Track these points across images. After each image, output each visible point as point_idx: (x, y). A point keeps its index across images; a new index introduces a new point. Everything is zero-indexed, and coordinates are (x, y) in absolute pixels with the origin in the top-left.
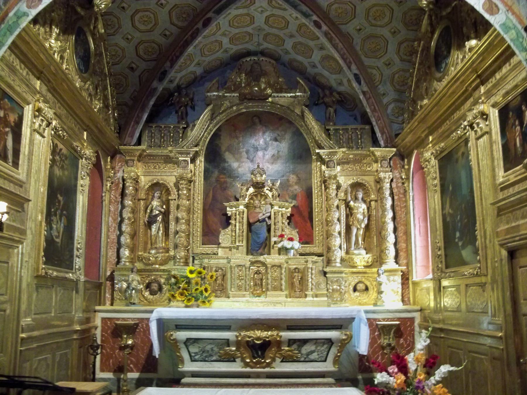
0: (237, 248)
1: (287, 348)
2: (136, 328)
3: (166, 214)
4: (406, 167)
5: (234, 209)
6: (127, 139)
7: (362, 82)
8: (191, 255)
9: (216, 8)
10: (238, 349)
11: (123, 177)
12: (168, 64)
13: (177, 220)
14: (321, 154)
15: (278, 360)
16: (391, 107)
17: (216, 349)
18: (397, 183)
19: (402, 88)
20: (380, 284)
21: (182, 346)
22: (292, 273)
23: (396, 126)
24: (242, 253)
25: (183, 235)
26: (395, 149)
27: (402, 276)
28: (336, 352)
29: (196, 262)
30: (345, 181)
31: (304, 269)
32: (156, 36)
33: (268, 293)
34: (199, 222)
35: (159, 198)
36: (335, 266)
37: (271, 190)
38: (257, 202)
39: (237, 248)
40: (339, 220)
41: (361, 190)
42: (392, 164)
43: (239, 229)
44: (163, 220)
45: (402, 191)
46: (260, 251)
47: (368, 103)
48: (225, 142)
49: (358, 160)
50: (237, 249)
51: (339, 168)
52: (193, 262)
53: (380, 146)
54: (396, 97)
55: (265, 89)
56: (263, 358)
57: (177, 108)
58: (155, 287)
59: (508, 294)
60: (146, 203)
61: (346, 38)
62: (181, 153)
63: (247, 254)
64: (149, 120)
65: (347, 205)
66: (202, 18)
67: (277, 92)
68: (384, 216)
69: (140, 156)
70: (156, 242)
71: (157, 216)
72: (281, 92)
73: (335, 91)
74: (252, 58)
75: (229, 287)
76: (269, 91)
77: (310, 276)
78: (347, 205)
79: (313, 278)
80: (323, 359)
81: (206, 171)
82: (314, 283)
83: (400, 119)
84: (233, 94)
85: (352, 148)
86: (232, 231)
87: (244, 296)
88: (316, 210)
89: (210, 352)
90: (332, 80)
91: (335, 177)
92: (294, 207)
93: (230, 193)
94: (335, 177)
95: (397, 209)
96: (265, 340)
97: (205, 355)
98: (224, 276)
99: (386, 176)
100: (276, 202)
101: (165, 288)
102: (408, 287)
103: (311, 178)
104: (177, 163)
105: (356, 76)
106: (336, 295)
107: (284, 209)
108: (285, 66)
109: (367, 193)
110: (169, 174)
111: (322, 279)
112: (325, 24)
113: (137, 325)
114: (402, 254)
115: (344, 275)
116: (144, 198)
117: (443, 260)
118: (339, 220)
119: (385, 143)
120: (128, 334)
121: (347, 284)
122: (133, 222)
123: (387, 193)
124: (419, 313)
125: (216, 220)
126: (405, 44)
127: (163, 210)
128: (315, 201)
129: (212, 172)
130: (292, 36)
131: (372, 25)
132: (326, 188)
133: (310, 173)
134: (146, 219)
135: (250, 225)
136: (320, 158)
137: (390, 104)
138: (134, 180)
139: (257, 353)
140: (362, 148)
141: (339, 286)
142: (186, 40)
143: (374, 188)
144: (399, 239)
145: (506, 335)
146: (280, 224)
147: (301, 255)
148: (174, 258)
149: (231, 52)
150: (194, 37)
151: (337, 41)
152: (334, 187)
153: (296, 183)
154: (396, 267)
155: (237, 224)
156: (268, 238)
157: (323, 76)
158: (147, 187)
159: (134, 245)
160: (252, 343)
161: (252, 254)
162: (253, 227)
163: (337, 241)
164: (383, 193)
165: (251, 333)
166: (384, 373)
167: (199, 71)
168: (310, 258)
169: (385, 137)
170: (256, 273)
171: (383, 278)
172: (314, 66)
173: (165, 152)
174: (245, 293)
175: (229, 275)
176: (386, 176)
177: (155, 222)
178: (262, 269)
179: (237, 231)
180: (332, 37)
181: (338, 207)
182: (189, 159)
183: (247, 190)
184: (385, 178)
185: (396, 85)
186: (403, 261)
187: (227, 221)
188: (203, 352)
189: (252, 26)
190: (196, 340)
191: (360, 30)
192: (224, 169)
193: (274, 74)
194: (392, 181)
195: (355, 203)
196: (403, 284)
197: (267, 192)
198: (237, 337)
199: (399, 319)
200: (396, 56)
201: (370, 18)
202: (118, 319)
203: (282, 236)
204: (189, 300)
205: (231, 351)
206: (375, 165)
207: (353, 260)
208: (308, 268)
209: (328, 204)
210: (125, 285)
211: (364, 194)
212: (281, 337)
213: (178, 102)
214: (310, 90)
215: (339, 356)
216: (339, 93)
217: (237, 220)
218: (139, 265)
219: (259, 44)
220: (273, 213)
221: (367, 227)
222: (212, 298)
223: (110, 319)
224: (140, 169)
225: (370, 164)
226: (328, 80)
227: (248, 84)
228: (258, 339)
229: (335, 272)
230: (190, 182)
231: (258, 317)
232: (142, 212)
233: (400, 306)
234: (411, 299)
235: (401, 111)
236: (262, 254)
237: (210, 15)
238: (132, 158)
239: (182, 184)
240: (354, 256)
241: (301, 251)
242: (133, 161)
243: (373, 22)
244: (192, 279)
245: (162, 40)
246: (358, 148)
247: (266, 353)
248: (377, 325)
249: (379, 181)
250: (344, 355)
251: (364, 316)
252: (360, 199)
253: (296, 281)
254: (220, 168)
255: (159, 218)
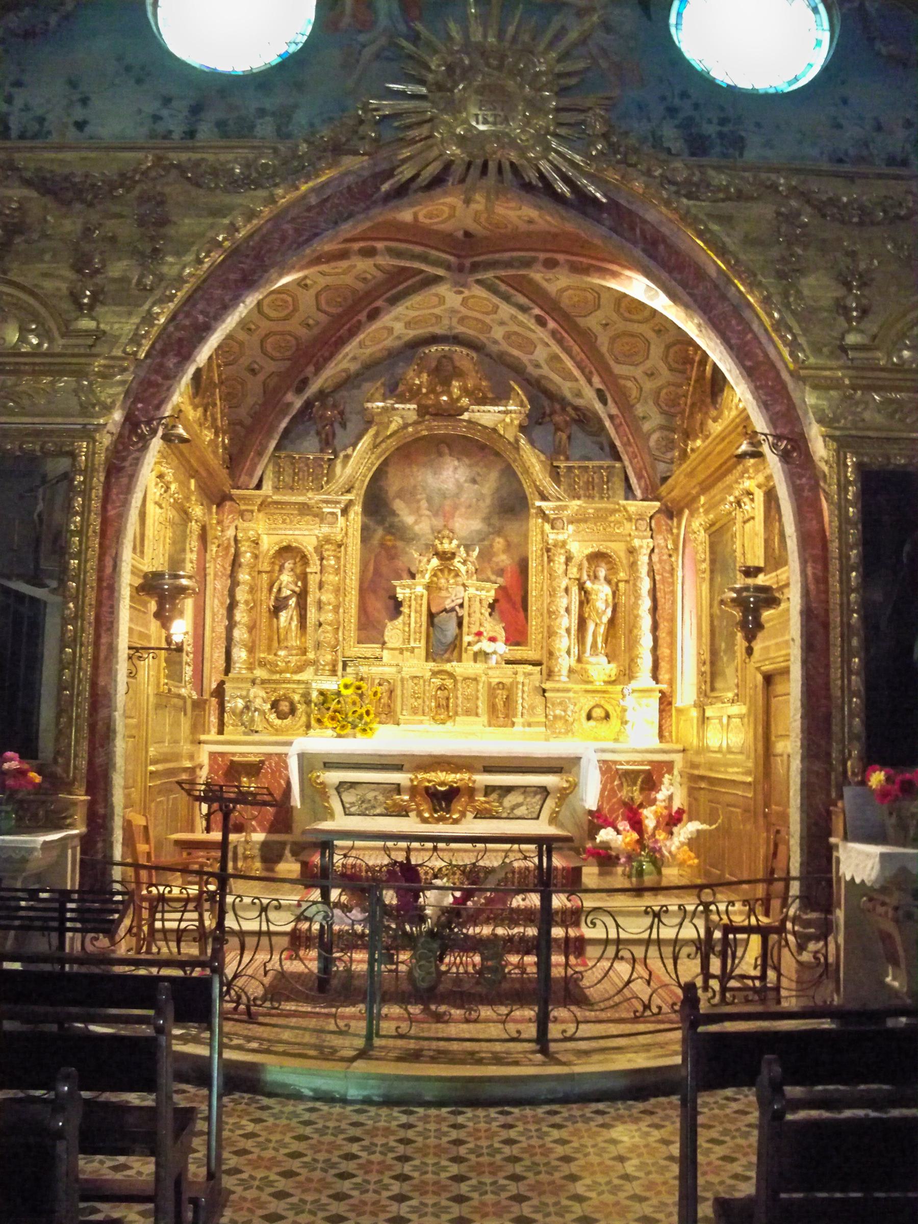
0: (412, 650)
1: (483, 799)
2: (261, 768)
3: (302, 596)
4: (675, 531)
5: (408, 591)
6: (243, 478)
7: (610, 401)
8: (340, 659)
9: (388, 295)
10: (413, 798)
11: (236, 537)
12: (311, 368)
13: (320, 605)
14: (544, 508)
15: (470, 816)
16: (655, 437)
17: (381, 798)
18: (661, 554)
19: (672, 410)
20: (624, 710)
21: (333, 793)
22: (492, 691)
23: (662, 467)
24: (419, 659)
25: (329, 628)
26: (658, 504)
27: (660, 699)
28: (554, 806)
29: (349, 670)
30: (579, 549)
31: (512, 683)
32: (294, 326)
33: (457, 718)
34: (353, 610)
35: (292, 570)
36: (558, 681)
37: (464, 563)
38: (443, 581)
39: (412, 650)
40: (567, 610)
41: (603, 565)
42: (653, 525)
43: (416, 622)
44: (298, 604)
45: (667, 568)
46: (446, 656)
47: (617, 432)
48: (393, 484)
49: (601, 517)
50: (412, 652)
51: (571, 528)
52: (344, 669)
53: (634, 498)
54: (663, 422)
55: (458, 399)
56: (448, 811)
57: (320, 427)
58: (284, 706)
59: (760, 730)
60: (270, 578)
61: (586, 338)
62: (327, 502)
63: (427, 661)
64: (278, 448)
65: (582, 587)
66: (366, 306)
67: (479, 404)
68: (636, 606)
69: (261, 505)
70: (286, 639)
71: (287, 598)
72: (485, 404)
73: (570, 404)
74: (440, 348)
75: (399, 709)
76: (465, 401)
77: (520, 694)
78: (582, 587)
79: (524, 699)
80: (535, 816)
81: (365, 528)
82: (525, 705)
83: (669, 456)
84: (408, 406)
85: (593, 497)
86: (404, 624)
87: (421, 722)
88: (533, 593)
89: (373, 802)
90: (566, 389)
91: (564, 543)
92: (502, 589)
93: (400, 564)
94: (564, 543)
95: (659, 595)
96: (451, 787)
97: (364, 806)
98: (391, 692)
99: (643, 544)
100: (472, 581)
101: (301, 708)
102: (671, 716)
103: (527, 543)
104: (320, 517)
105: (599, 393)
106: (559, 724)
107: (484, 593)
108: (491, 358)
109: (612, 568)
110: (306, 533)
111: (539, 699)
112: (553, 319)
113: (262, 762)
114: (664, 665)
115: (571, 694)
116: (268, 569)
117: (708, 680)
118: (567, 610)
119: (643, 493)
120: (248, 775)
121: (577, 709)
122: (252, 608)
123: (643, 570)
124: (681, 755)
125: (379, 605)
126: (675, 348)
127: (297, 589)
128: (532, 579)
129: (375, 531)
130: (502, 323)
131: (626, 320)
132: (550, 560)
133: (526, 537)
134: (272, 603)
135: (431, 616)
136: (542, 513)
137: (654, 431)
138: (253, 541)
139: (440, 805)
140: (608, 498)
141: (565, 711)
142: (340, 337)
143: (624, 561)
144: (660, 642)
145: (755, 781)
146: (478, 615)
147: (508, 662)
148: (314, 663)
149: (406, 338)
150: (352, 333)
151: (572, 343)
152: (562, 559)
153: (504, 552)
154: (652, 684)
155: (413, 614)
156: (459, 637)
157: (551, 380)
158: (272, 552)
159: (254, 642)
160: (432, 790)
161: (434, 661)
162: (436, 620)
163: (563, 643)
164: (637, 570)
165: (431, 776)
166: (610, 830)
167: (354, 367)
168: (520, 668)
169: (643, 484)
170: (440, 688)
171: (630, 702)
172: (538, 366)
173: (301, 499)
174: (423, 718)
175: (398, 692)
176: (643, 544)
177: (286, 607)
178: (449, 683)
179: (413, 625)
180: (563, 337)
181: (567, 590)
182: (338, 511)
183: (429, 561)
184: (641, 547)
185: (663, 405)
186: (664, 675)
187: (396, 608)
188: (363, 802)
189: (442, 307)
190: (353, 785)
191: (607, 325)
192: (392, 526)
193: (474, 374)
194: (653, 550)
195: (593, 583)
196: (661, 711)
197: (459, 565)
198: (412, 780)
199: (651, 763)
200: (662, 364)
201: (622, 310)
202: (234, 754)
203: (479, 634)
204: (343, 727)
205: (403, 800)
206: (628, 525)
207: (586, 671)
208: (518, 683)
209: (551, 585)
210: (240, 704)
211: (609, 570)
212: (474, 782)
213: (321, 417)
214: (531, 401)
215: (557, 813)
216: (576, 409)
217: (413, 608)
218: (260, 673)
219: (451, 328)
220: (466, 599)
221: (612, 622)
222: (374, 726)
223: (222, 754)
224: (261, 523)
225: (619, 523)
226: (560, 388)
227: (432, 391)
228: (442, 784)
229: (558, 690)
230: (340, 546)
231: (443, 753)
232: (265, 592)
233: (656, 744)
234: (674, 734)
235: (670, 445)
236: (449, 661)
237: (379, 303)
238: (249, 508)
239: (327, 550)
240: (588, 666)
241: (509, 657)
242: (252, 512)
243: (627, 315)
244: (347, 696)
245: (303, 332)
246: (602, 498)
247: (453, 806)
248: (617, 770)
249: (632, 551)
250: (565, 813)
251: (595, 757)
252: (602, 578)
253: (500, 704)
254: (387, 525)
255: (292, 602)
